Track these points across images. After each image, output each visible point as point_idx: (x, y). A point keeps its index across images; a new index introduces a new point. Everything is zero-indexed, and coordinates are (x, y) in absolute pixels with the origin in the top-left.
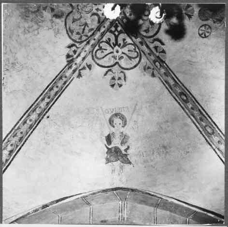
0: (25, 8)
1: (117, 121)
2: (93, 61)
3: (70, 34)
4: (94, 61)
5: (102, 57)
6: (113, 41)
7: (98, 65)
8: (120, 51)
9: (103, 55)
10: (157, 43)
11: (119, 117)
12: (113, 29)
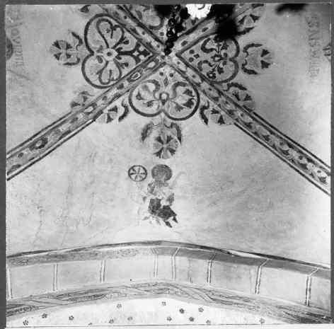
5: (101, 31)
6: (125, 48)
7: (89, 24)
9: (104, 33)
10: (121, 111)
12: (142, 48)
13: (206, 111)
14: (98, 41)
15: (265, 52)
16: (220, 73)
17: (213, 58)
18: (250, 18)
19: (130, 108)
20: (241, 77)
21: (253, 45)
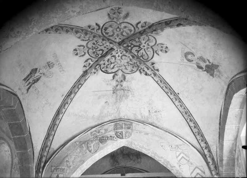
0: (123, 97)
1: (190, 57)
2: (150, 61)
3: (133, 72)
4: (149, 60)
5: (147, 56)
6: (137, 48)
7: (152, 58)
8: (143, 44)
9: (146, 55)
10: (139, 26)
11: (187, 55)
12: (130, 48)
13: (98, 28)
14: (148, 52)
15: (77, 54)
16: (94, 43)
17: (98, 48)
18: (86, 66)
19: (135, 26)
20: (84, 43)
21: (83, 56)
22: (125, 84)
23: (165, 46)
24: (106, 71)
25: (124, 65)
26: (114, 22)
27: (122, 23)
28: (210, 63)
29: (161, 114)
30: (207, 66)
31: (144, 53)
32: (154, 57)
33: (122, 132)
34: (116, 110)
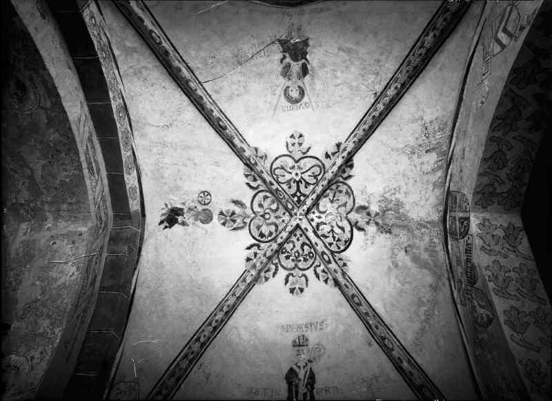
1: (295, 94)
2: (324, 162)
3: (349, 190)
6: (302, 186)
7: (317, 159)
8: (293, 175)
10: (254, 184)
12: (302, 198)
15: (302, 290)
17: (297, 252)
19: (257, 191)
21: (307, 280)
22: (374, 208)
23: (291, 141)
24: (346, 242)
25: (337, 209)
26: (252, 223)
27: (252, 210)
28: (285, 57)
29: (431, 122)
30: (296, 60)
31: (309, 173)
32: (313, 155)
33: (461, 219)
34: (423, 230)
